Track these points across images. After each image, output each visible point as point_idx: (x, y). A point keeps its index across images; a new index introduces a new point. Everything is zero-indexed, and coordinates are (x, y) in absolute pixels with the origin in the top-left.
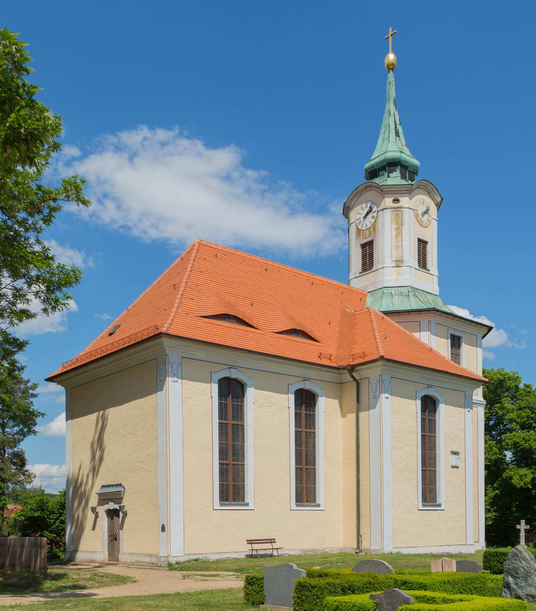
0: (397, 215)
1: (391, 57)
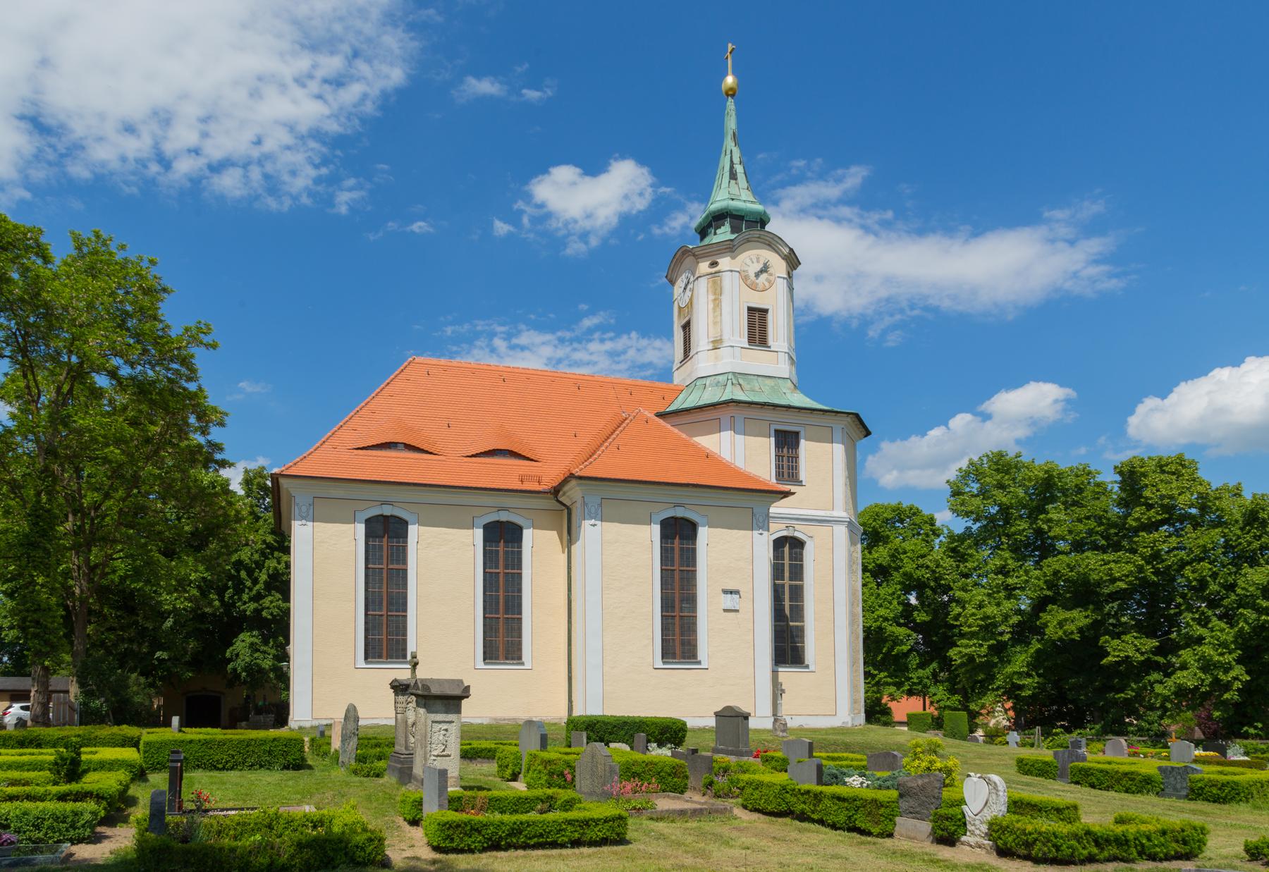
0: (714, 282)
1: (730, 80)
